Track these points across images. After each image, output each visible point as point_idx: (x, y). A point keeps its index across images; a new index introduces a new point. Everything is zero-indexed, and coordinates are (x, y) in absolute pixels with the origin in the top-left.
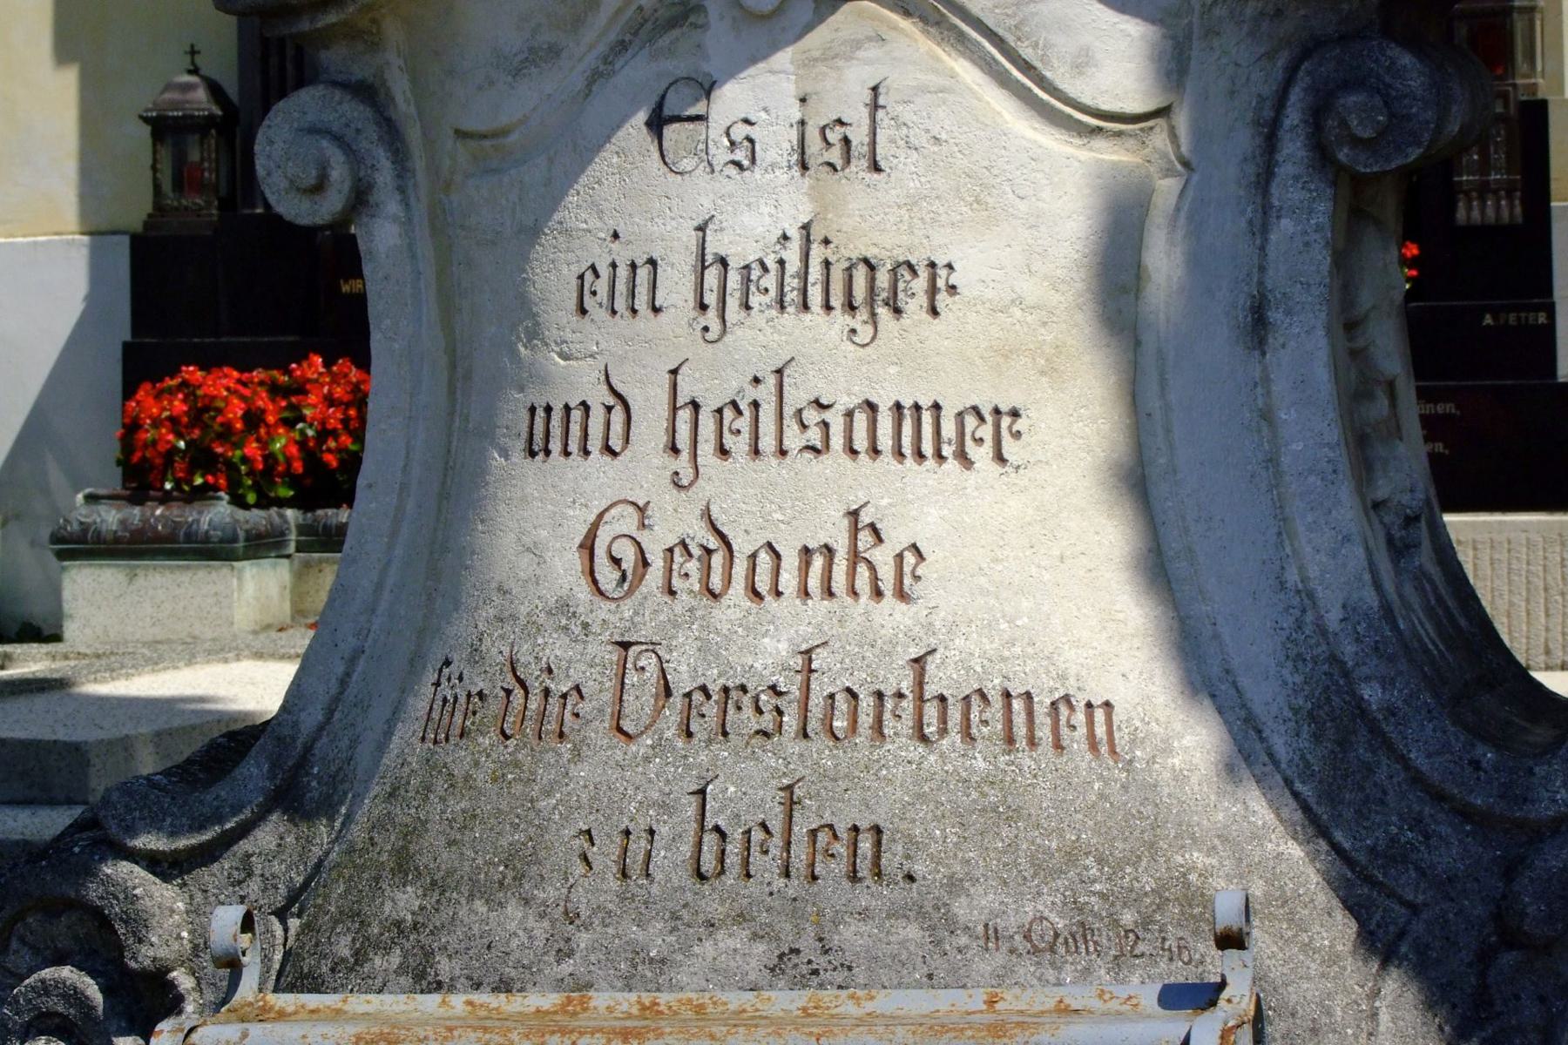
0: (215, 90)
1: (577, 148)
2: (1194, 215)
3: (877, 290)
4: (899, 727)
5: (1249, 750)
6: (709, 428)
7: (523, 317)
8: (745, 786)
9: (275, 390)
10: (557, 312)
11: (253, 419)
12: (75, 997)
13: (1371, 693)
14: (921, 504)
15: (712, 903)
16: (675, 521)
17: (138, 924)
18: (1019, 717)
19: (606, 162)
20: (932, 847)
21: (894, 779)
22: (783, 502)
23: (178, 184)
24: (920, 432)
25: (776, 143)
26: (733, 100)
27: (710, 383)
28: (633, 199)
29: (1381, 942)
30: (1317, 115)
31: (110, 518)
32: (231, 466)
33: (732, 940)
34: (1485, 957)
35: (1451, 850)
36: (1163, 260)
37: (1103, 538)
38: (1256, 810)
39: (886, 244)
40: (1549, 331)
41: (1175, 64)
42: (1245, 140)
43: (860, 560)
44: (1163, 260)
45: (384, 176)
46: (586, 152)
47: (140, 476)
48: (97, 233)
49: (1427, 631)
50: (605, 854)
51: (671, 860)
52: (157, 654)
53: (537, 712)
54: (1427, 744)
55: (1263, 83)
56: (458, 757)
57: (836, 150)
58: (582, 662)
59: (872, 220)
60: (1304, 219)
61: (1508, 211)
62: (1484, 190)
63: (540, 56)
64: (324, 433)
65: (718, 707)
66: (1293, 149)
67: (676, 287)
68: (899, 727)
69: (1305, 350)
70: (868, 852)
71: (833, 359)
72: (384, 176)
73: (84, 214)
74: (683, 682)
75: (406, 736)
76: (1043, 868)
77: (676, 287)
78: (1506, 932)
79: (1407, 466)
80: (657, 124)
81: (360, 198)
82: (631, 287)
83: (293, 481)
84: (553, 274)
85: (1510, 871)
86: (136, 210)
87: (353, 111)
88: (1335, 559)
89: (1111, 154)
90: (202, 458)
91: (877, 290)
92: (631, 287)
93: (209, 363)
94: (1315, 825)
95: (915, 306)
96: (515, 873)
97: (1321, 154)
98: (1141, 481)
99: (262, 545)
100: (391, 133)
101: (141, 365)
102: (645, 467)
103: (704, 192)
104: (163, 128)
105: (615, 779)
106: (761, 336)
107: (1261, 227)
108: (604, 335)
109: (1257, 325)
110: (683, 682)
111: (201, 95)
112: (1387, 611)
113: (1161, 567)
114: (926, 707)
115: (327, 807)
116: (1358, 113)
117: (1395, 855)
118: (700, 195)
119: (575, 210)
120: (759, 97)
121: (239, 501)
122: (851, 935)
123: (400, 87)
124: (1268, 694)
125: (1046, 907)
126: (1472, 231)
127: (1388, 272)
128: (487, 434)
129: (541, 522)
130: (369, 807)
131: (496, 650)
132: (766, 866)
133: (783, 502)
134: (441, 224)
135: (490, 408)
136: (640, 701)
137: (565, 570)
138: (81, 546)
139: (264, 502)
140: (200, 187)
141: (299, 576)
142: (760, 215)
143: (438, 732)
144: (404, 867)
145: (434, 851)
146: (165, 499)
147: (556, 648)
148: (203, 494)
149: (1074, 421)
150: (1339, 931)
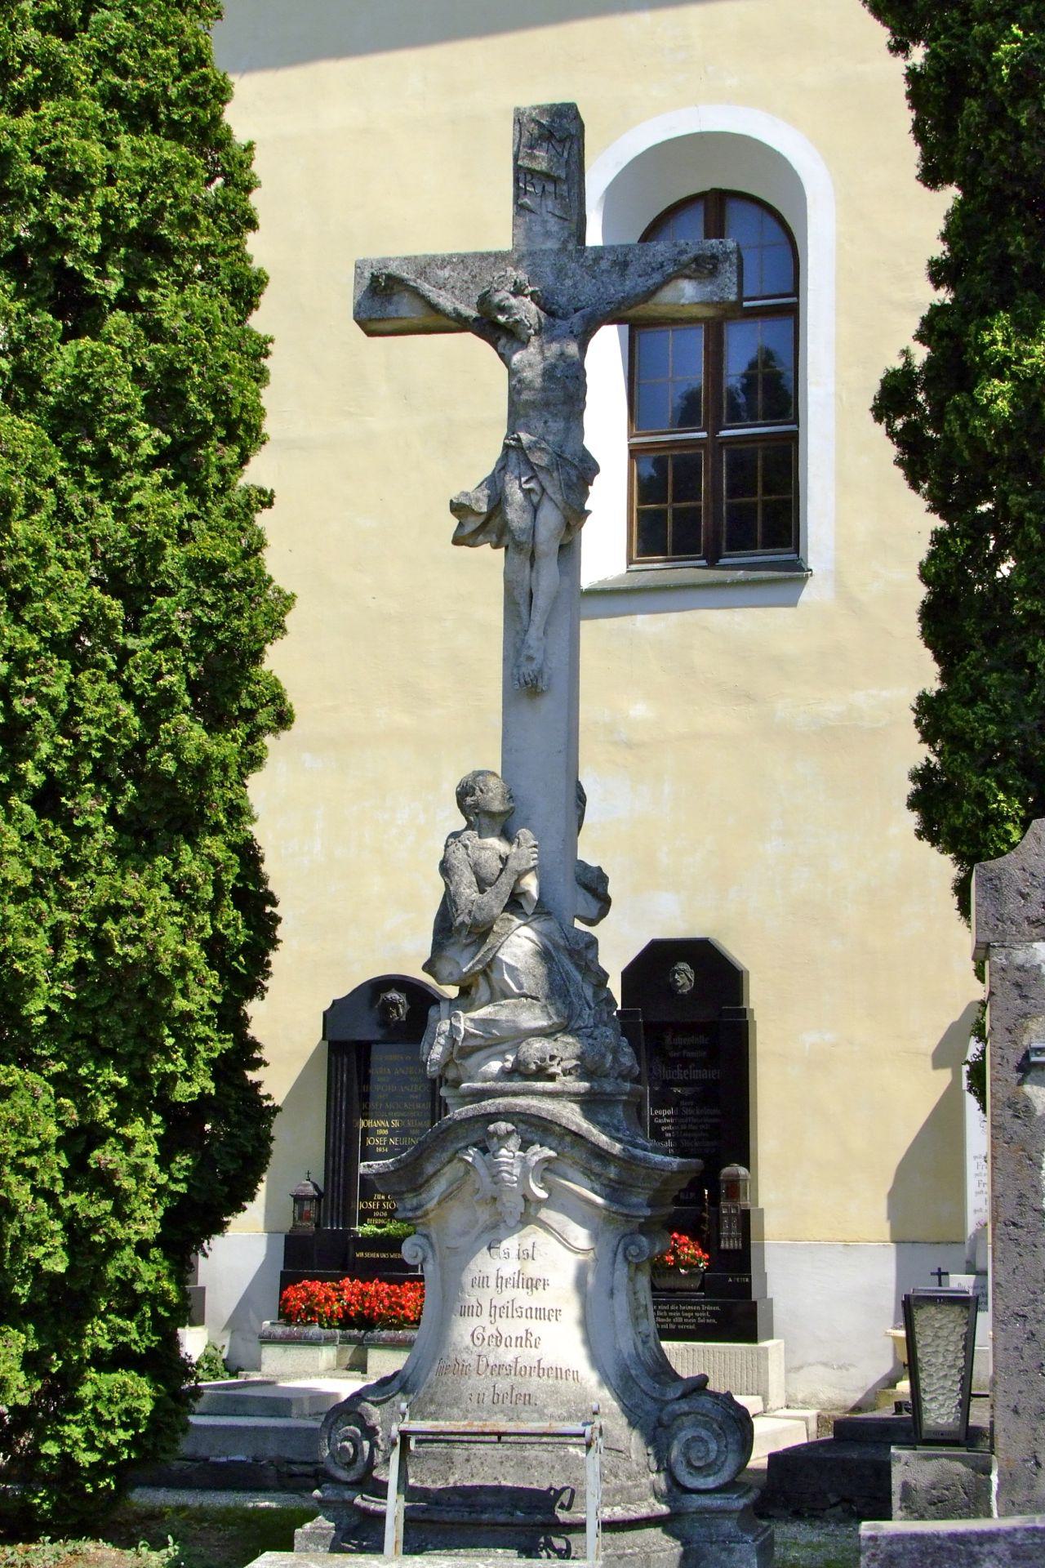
0: (316, 1187)
1: (472, 1253)
2: (597, 1273)
3: (532, 1284)
4: (534, 1374)
5: (605, 1380)
6: (497, 1312)
7: (460, 1287)
8: (503, 1385)
9: (334, 1289)
10: (468, 1287)
11: (328, 1299)
12: (354, 1433)
13: (633, 1372)
14: (538, 1327)
15: (496, 1409)
16: (491, 1330)
17: (370, 1416)
18: (559, 1373)
19: (479, 1256)
20: (541, 1398)
21: (534, 1384)
22: (512, 1327)
23: (300, 1218)
24: (541, 1314)
25: (513, 1254)
26: (505, 1244)
27: (498, 1303)
28: (485, 1264)
29: (632, 1424)
30: (625, 1249)
31: (279, 1330)
32: (320, 1315)
33: (500, 1416)
34: (655, 1428)
35: (649, 1405)
36: (591, 1278)
37: (575, 1335)
38: (606, 1393)
39: (535, 1276)
40: (750, 1283)
41: (595, 1237)
42: (611, 1255)
43: (526, 1339)
44: (591, 1278)
45: (430, 1255)
46: (475, 1253)
47: (286, 1315)
48: (271, 1232)
49: (650, 1361)
50: (474, 1398)
51: (488, 1400)
52: (298, 1376)
53: (462, 1370)
54: (645, 1383)
55: (615, 1242)
56: (444, 1378)
57: (525, 1256)
58: (471, 1359)
59: (532, 1270)
60: (622, 1272)
61: (736, 1244)
62: (729, 1238)
63: (465, 1233)
64: (349, 1305)
65: (498, 1369)
66: (620, 1257)
67: (492, 1282)
68: (534, 1374)
69: (622, 1300)
70: (528, 1399)
71: (524, 1298)
72: (430, 1255)
73: (265, 1227)
74: (491, 1363)
75: (432, 1376)
76: (562, 1403)
77: (492, 1282)
78: (660, 1423)
79: (649, 1325)
80: (489, 1248)
81: (424, 1259)
82: (483, 1282)
83: (339, 1320)
84: (467, 1279)
85: (661, 1410)
86: (288, 1225)
87: (423, 1241)
88: (626, 1342)
89: (581, 1257)
90: (311, 1311)
91: (532, 1284)
92: (483, 1282)
93: (313, 1278)
94: (619, 1398)
95: (540, 1288)
96: (456, 1402)
97: (625, 1256)
98: (585, 1323)
99: (329, 1341)
100: (432, 1245)
101: (288, 1279)
102: (485, 1320)
103: (498, 1263)
104: (298, 1199)
105: (477, 1383)
106: (509, 1293)
107: (613, 1274)
108: (477, 1292)
109: (612, 1294)
110: (491, 1363)
111: (311, 1188)
112: (638, 1355)
113: (588, 1341)
114: (540, 1370)
115: (412, 1391)
116: (633, 1250)
117: (637, 1406)
118: (499, 1263)
119: (472, 1265)
120: (510, 1244)
121: (321, 1326)
122: (524, 1415)
123: (434, 1236)
124: (611, 1371)
125: (563, 1411)
126: (726, 1251)
127: (644, 1281)
128: (452, 1311)
129: (463, 1330)
130: (423, 1389)
131: (453, 1356)
132: (507, 1401)
133: (512, 1327)
134: (442, 1265)
135: (452, 1304)
136: (482, 1368)
137: (468, 1340)
138: (268, 1340)
139: (330, 1327)
140: (308, 1219)
141: (340, 1352)
142: (509, 1268)
143: (440, 1372)
144: (432, 1401)
145: (438, 1398)
146: (298, 1325)
147: (465, 1356)
148: (310, 1323)
149: (571, 1310)
150: (623, 1421)
